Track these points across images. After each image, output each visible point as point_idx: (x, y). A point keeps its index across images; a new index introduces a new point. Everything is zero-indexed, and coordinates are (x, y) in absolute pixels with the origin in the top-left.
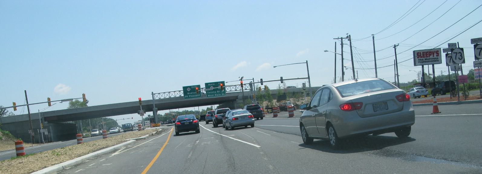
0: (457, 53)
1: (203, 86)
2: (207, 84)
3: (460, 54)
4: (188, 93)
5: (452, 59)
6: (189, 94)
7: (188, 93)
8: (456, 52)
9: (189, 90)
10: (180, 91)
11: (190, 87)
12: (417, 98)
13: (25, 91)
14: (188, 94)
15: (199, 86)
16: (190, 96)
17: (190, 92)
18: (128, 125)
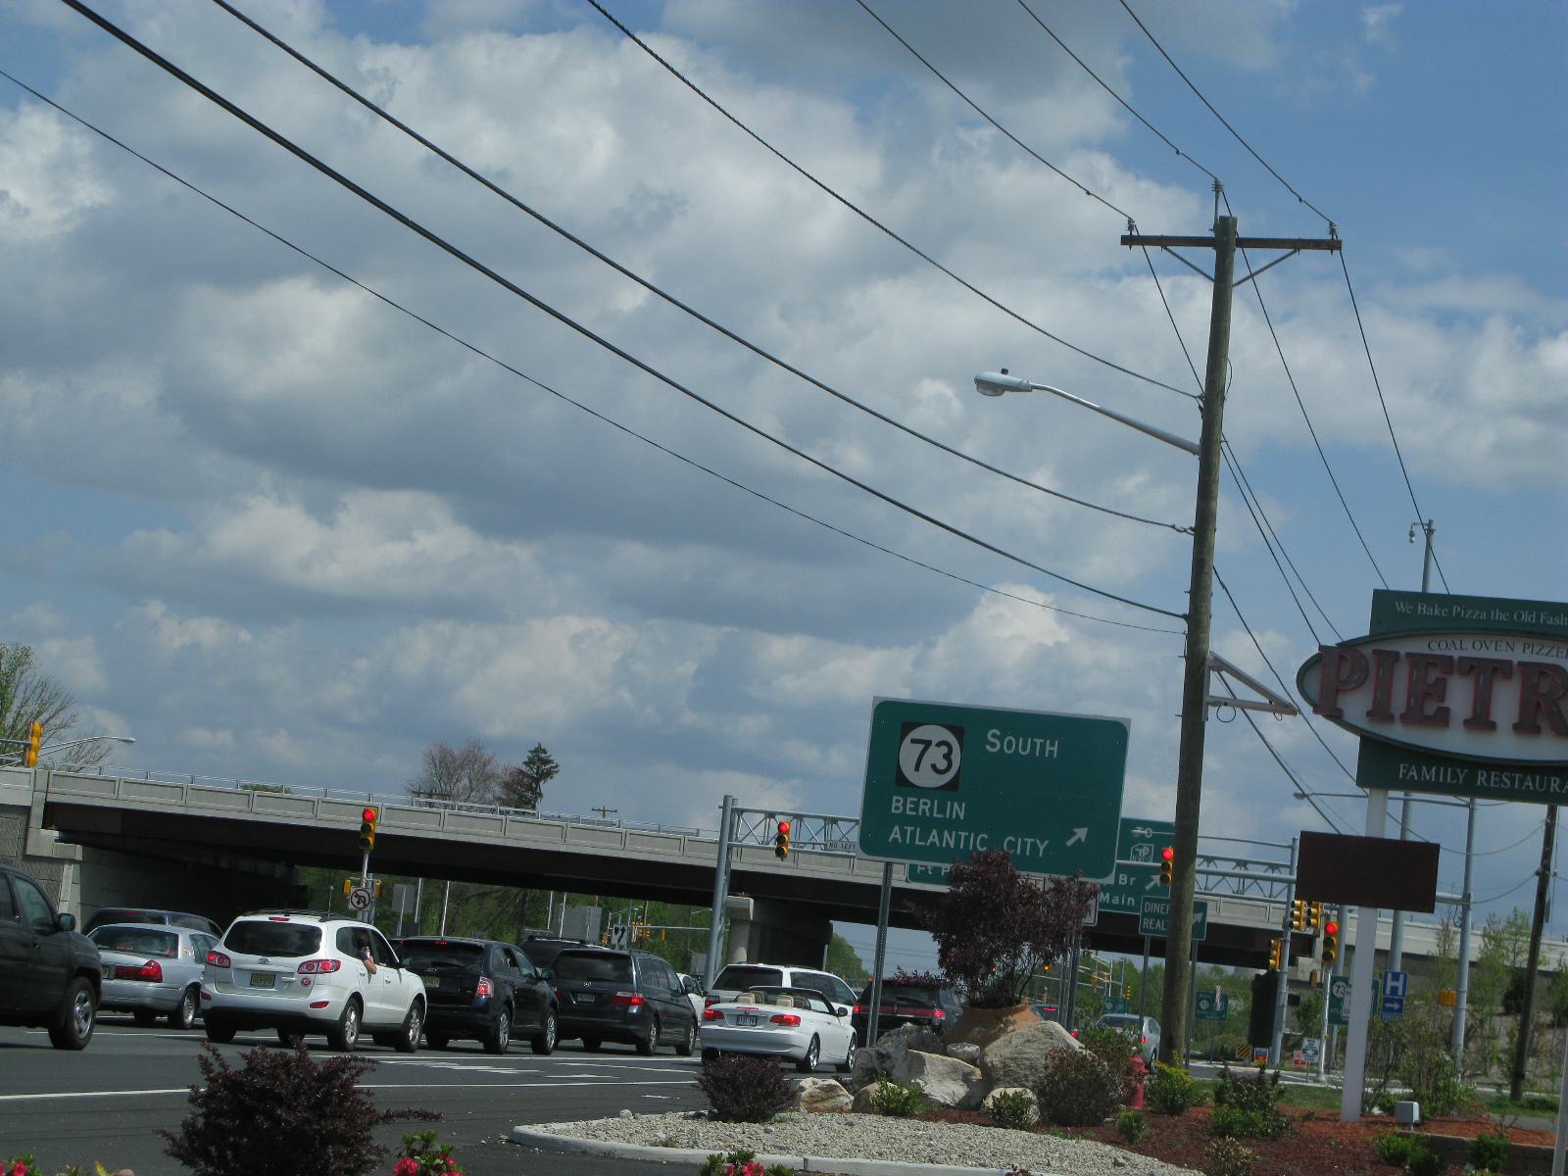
3: (944, 749)
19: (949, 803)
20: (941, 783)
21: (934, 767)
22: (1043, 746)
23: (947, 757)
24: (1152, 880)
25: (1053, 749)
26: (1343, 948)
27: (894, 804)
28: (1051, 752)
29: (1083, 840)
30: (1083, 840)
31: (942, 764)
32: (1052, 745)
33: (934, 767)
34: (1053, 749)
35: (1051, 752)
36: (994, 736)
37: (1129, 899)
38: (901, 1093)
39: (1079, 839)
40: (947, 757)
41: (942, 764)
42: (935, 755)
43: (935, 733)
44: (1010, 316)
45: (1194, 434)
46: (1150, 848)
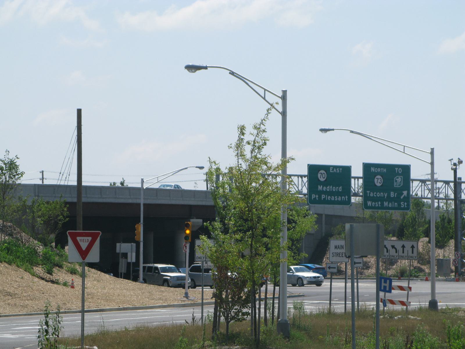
0: (378, 179)
1: (357, 171)
2: (367, 167)
3: (380, 179)
4: (320, 188)
5: (306, 187)
6: (323, 192)
7: (320, 188)
8: (321, 172)
9: (322, 177)
10: (302, 176)
11: (326, 168)
12: (278, 279)
13: (79, 111)
14: (320, 191)
15: (347, 170)
16: (323, 196)
17: (325, 184)
18: (457, 309)
19: (396, 196)
20: (375, 182)
21: (379, 182)
22: (383, 170)
23: (381, 181)
24: (403, 194)
25: (385, 170)
26: (435, 262)
27: (391, 194)
28: (385, 171)
29: (406, 196)
30: (406, 196)
31: (380, 182)
32: (385, 169)
33: (379, 182)
34: (385, 170)
35: (385, 171)
36: (402, 203)
37: (395, 204)
38: (232, 273)
39: (405, 196)
40: (381, 181)
41: (380, 182)
42: (379, 181)
43: (379, 177)
44: (411, 157)
45: (430, 161)
46: (401, 178)
